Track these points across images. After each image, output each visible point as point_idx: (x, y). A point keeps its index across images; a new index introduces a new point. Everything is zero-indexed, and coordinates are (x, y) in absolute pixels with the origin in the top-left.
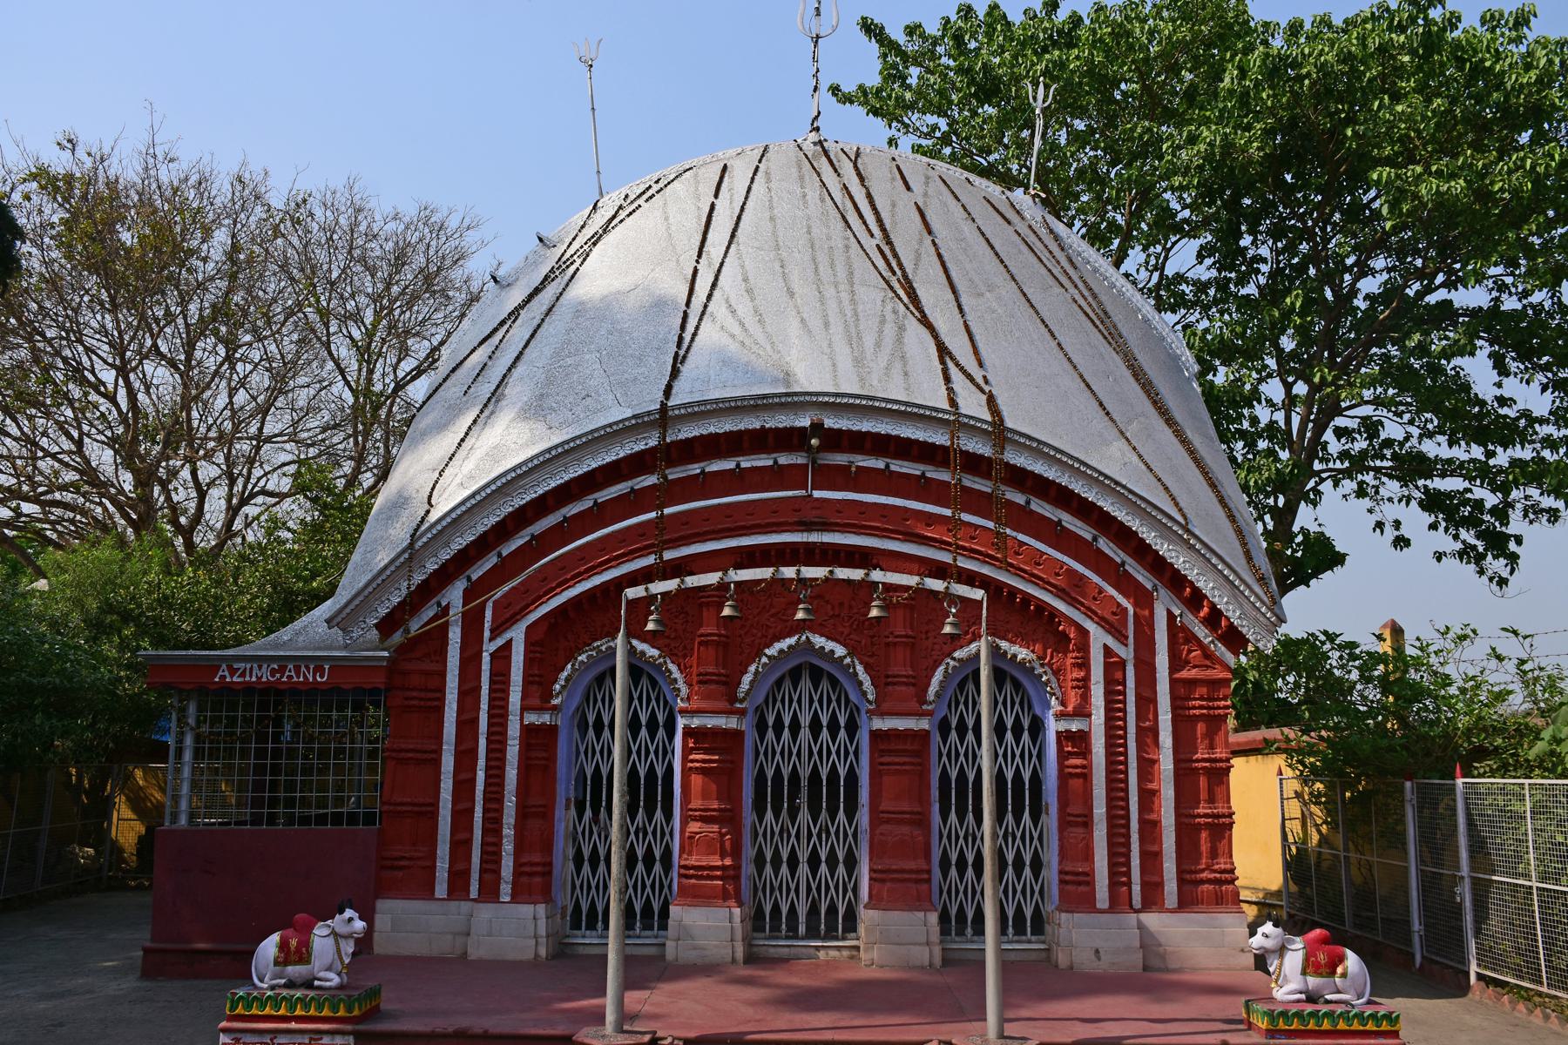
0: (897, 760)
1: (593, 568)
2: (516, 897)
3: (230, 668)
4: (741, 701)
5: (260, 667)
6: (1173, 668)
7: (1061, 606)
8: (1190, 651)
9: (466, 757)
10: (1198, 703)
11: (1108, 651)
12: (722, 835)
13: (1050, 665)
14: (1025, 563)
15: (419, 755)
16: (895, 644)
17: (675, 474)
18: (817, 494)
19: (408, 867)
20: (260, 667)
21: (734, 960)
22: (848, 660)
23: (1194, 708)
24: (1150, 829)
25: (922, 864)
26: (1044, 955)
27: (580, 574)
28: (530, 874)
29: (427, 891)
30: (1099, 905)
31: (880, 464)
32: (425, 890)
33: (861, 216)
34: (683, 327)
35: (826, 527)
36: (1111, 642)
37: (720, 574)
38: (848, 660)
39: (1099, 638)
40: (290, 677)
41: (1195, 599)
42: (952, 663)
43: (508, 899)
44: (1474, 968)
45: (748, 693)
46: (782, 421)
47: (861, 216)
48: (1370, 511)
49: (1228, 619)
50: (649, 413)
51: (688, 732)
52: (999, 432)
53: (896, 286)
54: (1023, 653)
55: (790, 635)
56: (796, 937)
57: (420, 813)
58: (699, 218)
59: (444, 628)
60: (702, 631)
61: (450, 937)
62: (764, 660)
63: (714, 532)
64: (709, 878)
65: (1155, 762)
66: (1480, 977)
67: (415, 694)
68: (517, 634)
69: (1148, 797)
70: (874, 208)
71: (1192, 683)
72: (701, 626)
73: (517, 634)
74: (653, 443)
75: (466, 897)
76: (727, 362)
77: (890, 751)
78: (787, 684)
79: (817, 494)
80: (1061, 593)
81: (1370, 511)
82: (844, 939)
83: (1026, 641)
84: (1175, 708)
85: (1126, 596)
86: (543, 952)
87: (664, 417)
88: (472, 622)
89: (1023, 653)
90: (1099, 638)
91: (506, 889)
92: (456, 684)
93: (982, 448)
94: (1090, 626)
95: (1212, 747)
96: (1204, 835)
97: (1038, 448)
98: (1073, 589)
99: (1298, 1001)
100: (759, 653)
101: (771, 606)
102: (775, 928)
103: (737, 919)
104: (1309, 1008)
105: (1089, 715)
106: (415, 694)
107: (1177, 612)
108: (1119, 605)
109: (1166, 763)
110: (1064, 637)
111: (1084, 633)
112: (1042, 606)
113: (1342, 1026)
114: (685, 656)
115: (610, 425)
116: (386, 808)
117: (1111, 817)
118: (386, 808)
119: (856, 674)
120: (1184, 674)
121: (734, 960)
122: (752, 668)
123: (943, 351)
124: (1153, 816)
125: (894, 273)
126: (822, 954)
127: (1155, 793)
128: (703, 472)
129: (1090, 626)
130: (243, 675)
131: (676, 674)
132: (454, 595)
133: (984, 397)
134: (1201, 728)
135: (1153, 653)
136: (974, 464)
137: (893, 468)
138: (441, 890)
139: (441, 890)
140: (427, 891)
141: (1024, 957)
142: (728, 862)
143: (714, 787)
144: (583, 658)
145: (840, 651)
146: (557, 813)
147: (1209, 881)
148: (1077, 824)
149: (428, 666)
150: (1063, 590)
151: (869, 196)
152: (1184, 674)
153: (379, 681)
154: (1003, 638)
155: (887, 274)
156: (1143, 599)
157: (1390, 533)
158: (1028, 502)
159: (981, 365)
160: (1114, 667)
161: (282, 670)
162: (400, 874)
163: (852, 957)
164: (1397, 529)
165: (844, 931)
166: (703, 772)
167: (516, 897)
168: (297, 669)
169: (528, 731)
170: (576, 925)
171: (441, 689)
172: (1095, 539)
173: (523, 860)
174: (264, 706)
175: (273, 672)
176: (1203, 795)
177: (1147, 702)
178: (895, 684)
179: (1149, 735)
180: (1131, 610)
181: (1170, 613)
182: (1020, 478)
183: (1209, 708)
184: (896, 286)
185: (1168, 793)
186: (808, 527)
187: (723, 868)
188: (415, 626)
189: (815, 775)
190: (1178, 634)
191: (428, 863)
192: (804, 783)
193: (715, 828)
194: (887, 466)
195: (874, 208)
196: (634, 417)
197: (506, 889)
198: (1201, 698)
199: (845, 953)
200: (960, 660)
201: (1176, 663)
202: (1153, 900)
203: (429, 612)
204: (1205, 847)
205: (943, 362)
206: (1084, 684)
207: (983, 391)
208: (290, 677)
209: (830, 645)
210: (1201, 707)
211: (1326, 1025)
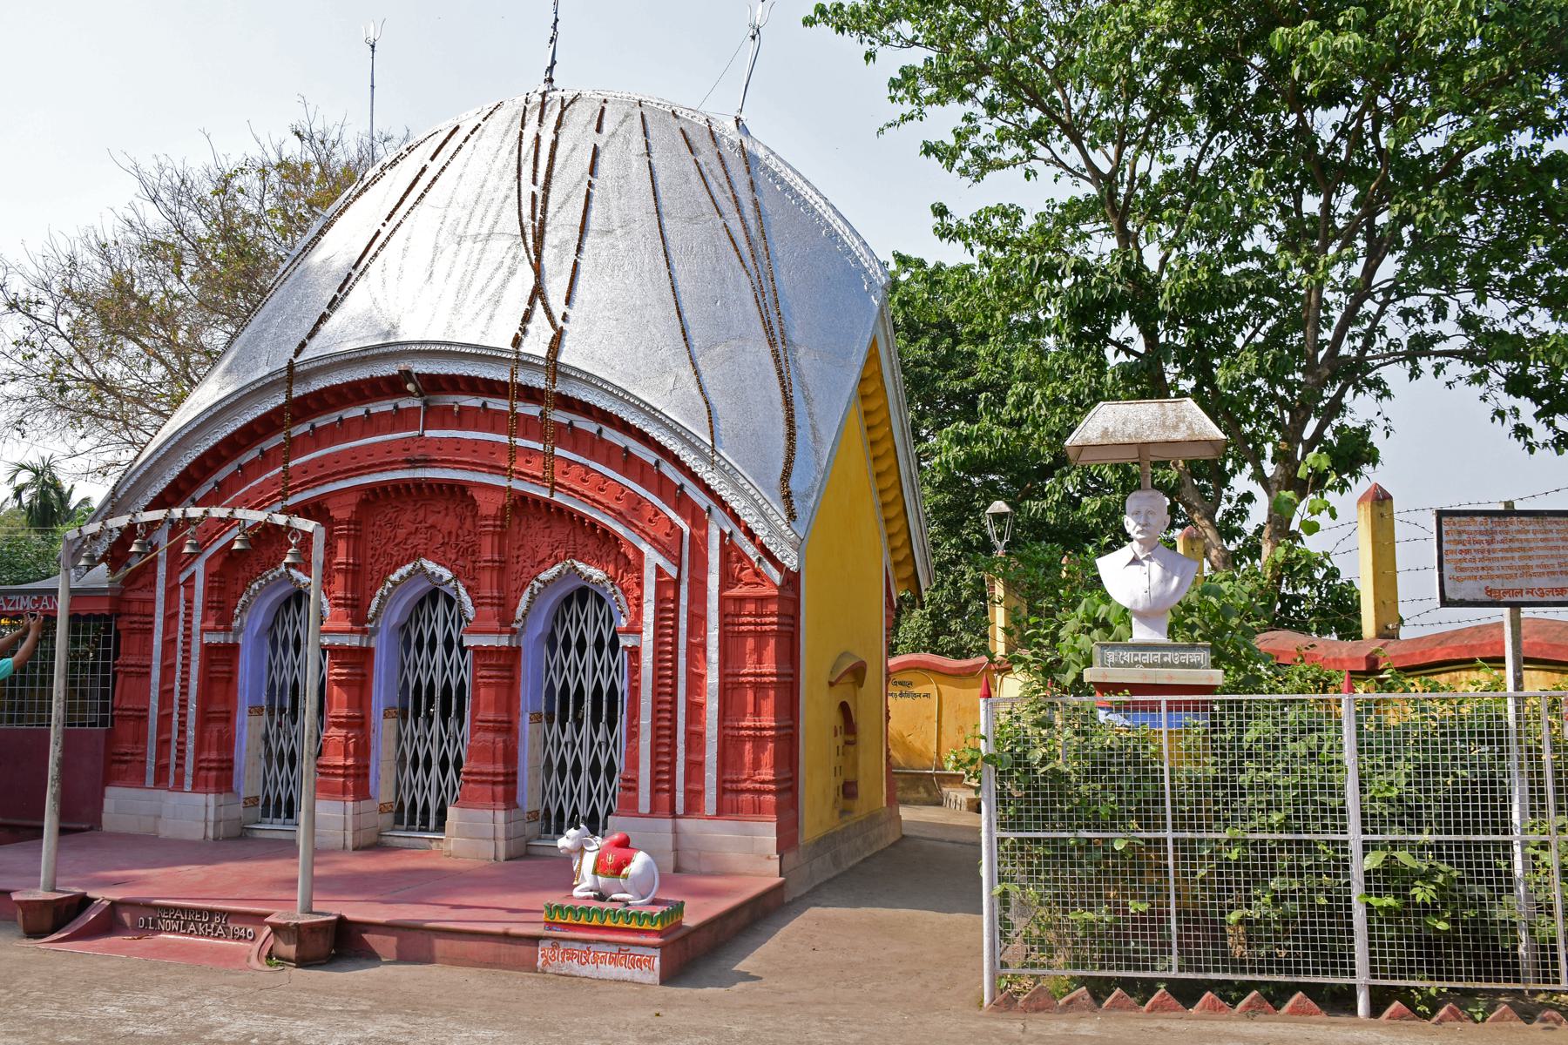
2: (195, 787)
4: (370, 622)
6: (724, 585)
7: (619, 529)
8: (742, 569)
10: (745, 620)
11: (659, 571)
12: (347, 739)
13: (620, 585)
14: (590, 489)
18: (429, 434)
21: (345, 847)
23: (772, 623)
24: (695, 740)
28: (209, 769)
30: (641, 810)
32: (139, 781)
33: (535, 171)
35: (427, 463)
36: (661, 561)
37: (129, 517)
38: (452, 584)
39: (652, 557)
41: (736, 518)
42: (537, 585)
45: (375, 615)
47: (535, 171)
48: (1484, 398)
50: (281, 371)
52: (552, 365)
53: (529, 231)
54: (597, 574)
55: (408, 562)
56: (427, 830)
62: (389, 585)
65: (702, 677)
69: (695, 710)
70: (552, 156)
71: (741, 600)
73: (199, 567)
74: (282, 400)
76: (370, 321)
78: (575, 606)
79: (429, 434)
80: (619, 516)
81: (1484, 398)
83: (598, 561)
84: (723, 625)
85: (683, 516)
86: (211, 834)
87: (292, 374)
89: (597, 574)
90: (652, 557)
91: (188, 781)
93: (539, 381)
94: (645, 548)
95: (760, 662)
96: (748, 746)
97: (588, 380)
98: (633, 510)
99: (588, 898)
100: (385, 578)
102: (412, 821)
103: (350, 812)
104: (596, 905)
105: (640, 632)
107: (727, 531)
108: (673, 525)
109: (712, 679)
111: (640, 554)
112: (606, 532)
113: (609, 923)
117: (656, 729)
120: (736, 592)
121: (345, 847)
122: (378, 593)
123: (538, 292)
124: (698, 728)
125: (533, 218)
126: (434, 844)
127: (701, 706)
128: (341, 419)
129: (645, 548)
133: (552, 332)
134: (750, 643)
135: (705, 571)
136: (530, 394)
137: (373, 411)
138: (150, 780)
139: (150, 780)
142: (500, 768)
144: (255, 586)
146: (238, 719)
147: (748, 791)
148: (220, 720)
149: (144, 595)
150: (620, 514)
151: (555, 144)
152: (736, 592)
154: (581, 560)
155: (527, 220)
156: (698, 518)
157: (1511, 421)
158: (600, 431)
159: (568, 301)
160: (667, 587)
161: (40, 600)
162: (124, 767)
164: (1517, 416)
166: (339, 683)
167: (195, 786)
169: (208, 649)
170: (265, 814)
172: (657, 463)
176: (750, 708)
177: (697, 620)
179: (697, 650)
180: (686, 530)
182: (568, 403)
183: (756, 624)
184: (529, 231)
185: (712, 706)
186: (412, 463)
187: (345, 767)
189: (447, 688)
190: (729, 551)
192: (437, 694)
193: (343, 732)
195: (552, 156)
196: (270, 374)
197: (188, 781)
198: (750, 615)
200: (545, 583)
201: (727, 580)
202: (693, 807)
204: (748, 758)
205: (531, 302)
207: (553, 325)
210: (749, 624)
211: (595, 922)
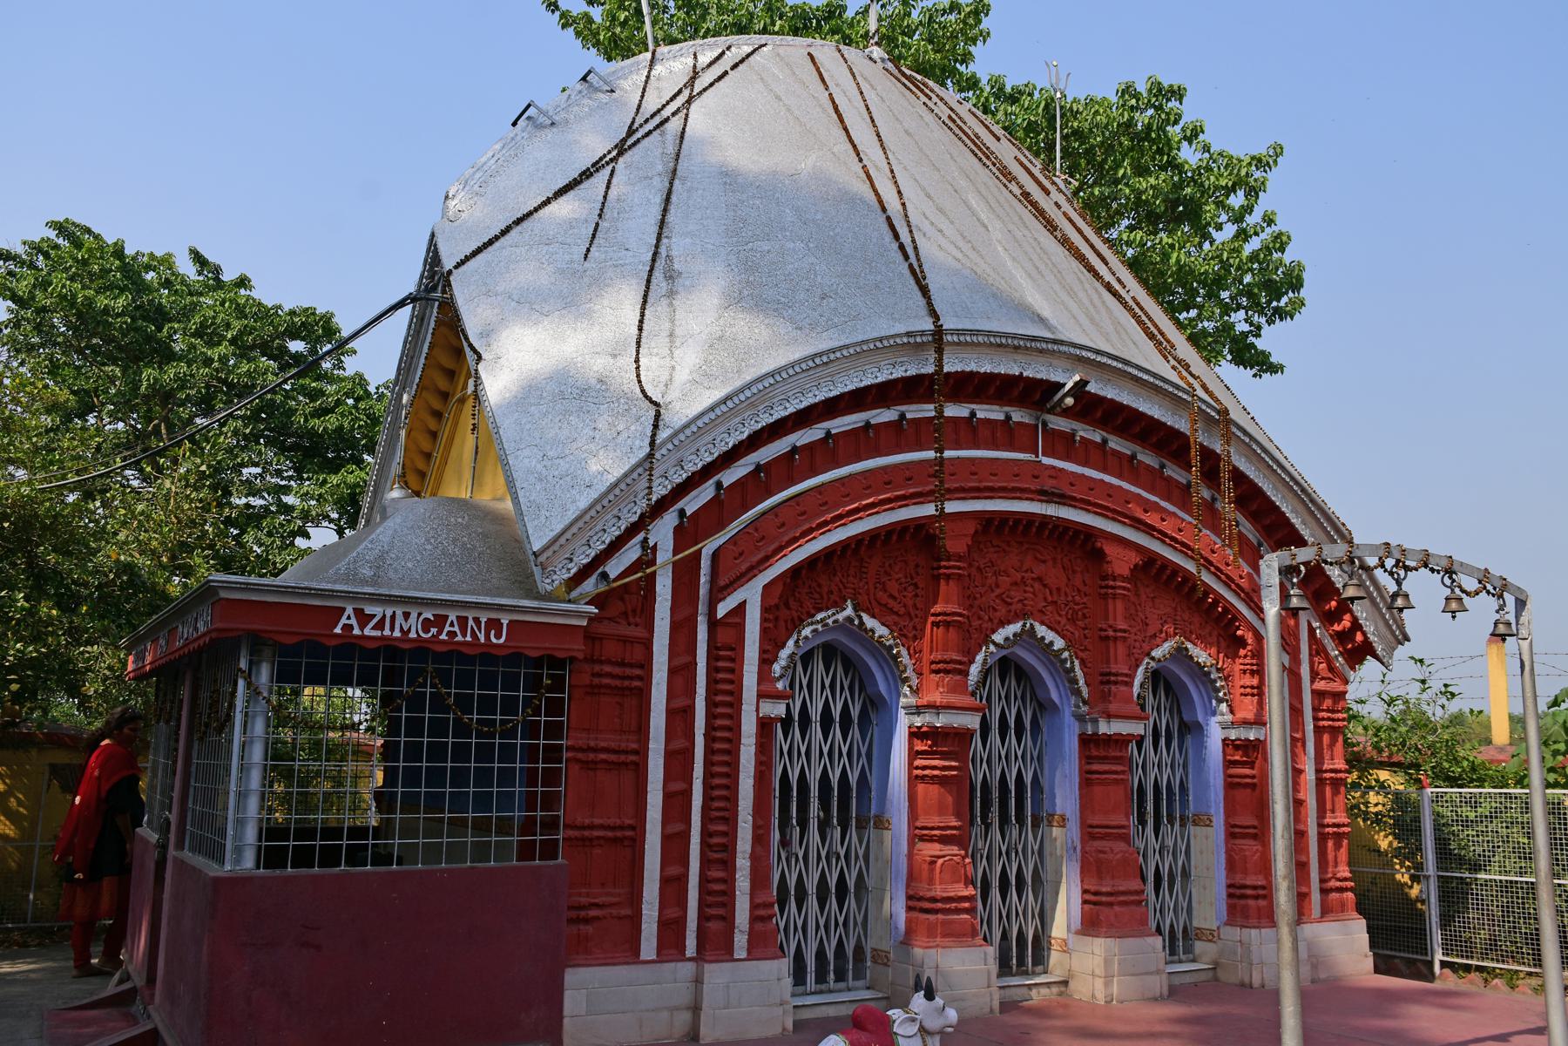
0: (1114, 768)
1: (840, 517)
3: (359, 613)
5: (407, 616)
9: (678, 761)
15: (613, 757)
16: (1116, 639)
17: (953, 411)
19: (597, 918)
20: (407, 616)
22: (1066, 654)
25: (1135, 884)
26: (1211, 974)
27: (826, 523)
29: (630, 951)
31: (1096, 436)
34: (896, 236)
38: (1066, 654)
40: (452, 634)
43: (744, 955)
44: (1439, 956)
46: (1037, 370)
49: (1364, 634)
51: (915, 734)
57: (615, 840)
58: (824, 110)
59: (652, 578)
60: (938, 608)
61: (666, 1014)
63: (963, 490)
64: (958, 911)
66: (1444, 964)
67: (608, 669)
68: (751, 594)
72: (935, 603)
73: (751, 594)
75: (680, 955)
77: (1105, 758)
82: (1034, 973)
88: (685, 573)
92: (666, 658)
100: (987, 640)
101: (997, 586)
106: (608, 669)
110: (1242, 642)
114: (915, 638)
115: (881, 340)
116: (571, 833)
118: (571, 833)
119: (1072, 669)
122: (979, 658)
130: (380, 626)
131: (905, 659)
132: (663, 532)
138: (648, 948)
139: (648, 948)
140: (630, 951)
141: (1188, 979)
143: (950, 799)
145: (1059, 643)
153: (577, 647)
161: (440, 621)
162: (589, 929)
163: (1061, 994)
165: (1034, 964)
168: (463, 621)
171: (647, 664)
173: (758, 901)
174: (534, 684)
175: (427, 625)
178: (1116, 683)
181: (1309, 624)
188: (614, 568)
191: (627, 911)
194: (1105, 441)
196: (908, 334)
198: (1328, 711)
199: (1055, 989)
203: (631, 553)
206: (1259, 692)
208: (452, 634)
209: (1050, 636)
